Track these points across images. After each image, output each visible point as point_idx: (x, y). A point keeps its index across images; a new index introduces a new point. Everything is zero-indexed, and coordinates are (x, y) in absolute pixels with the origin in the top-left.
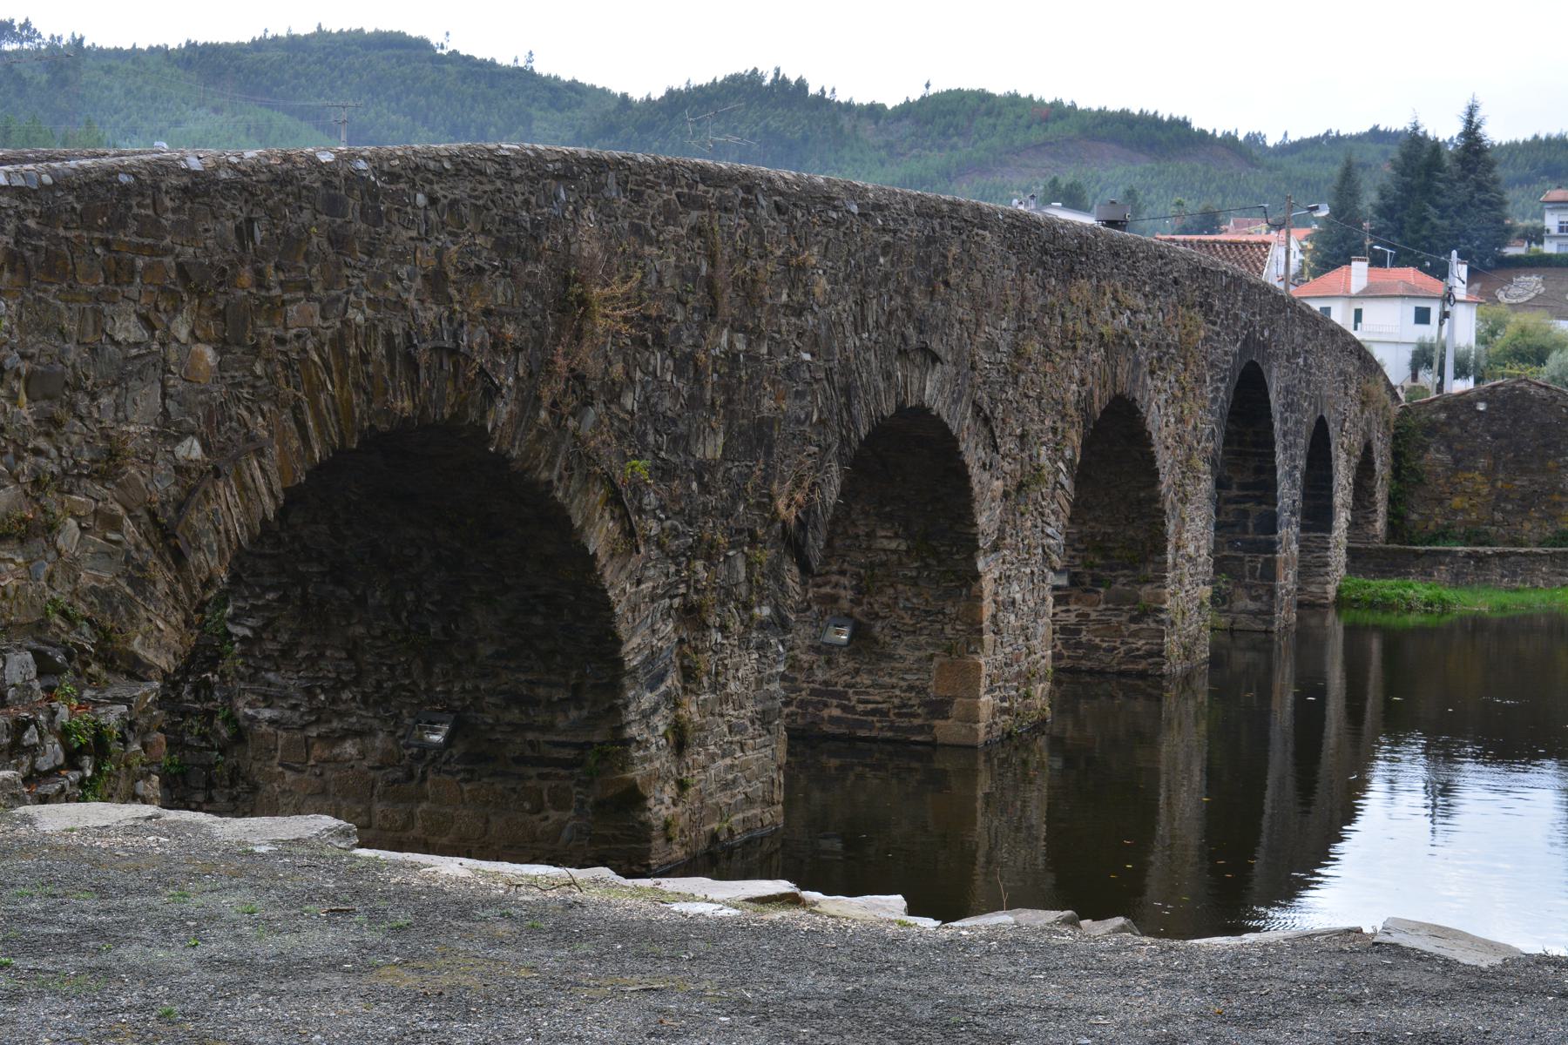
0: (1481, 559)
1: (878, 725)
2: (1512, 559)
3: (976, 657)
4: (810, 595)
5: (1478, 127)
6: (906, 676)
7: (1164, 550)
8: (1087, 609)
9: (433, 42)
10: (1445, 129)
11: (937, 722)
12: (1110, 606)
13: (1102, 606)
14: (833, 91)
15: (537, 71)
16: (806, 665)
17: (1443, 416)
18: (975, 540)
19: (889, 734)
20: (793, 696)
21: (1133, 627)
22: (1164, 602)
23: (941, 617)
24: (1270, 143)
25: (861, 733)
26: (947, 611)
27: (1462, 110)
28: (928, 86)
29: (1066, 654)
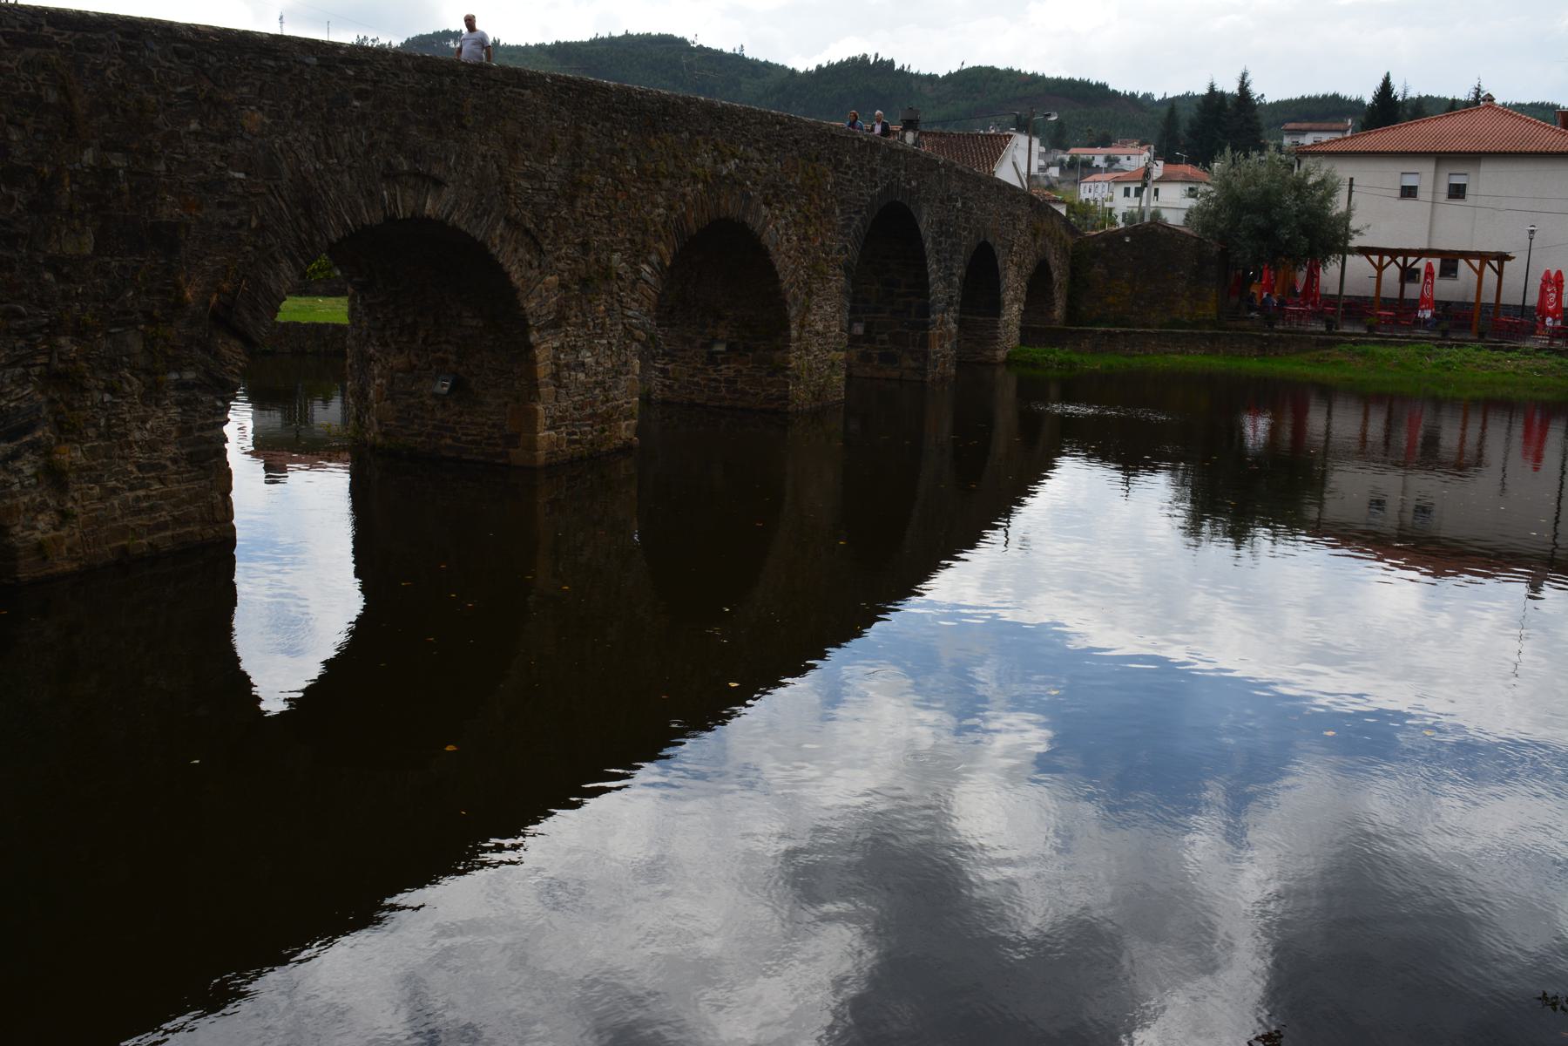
0: (1112, 335)
1: (475, 451)
2: (1133, 335)
3: (534, 404)
4: (430, 358)
5: (1247, 85)
6: (491, 417)
7: (788, 328)
8: (740, 367)
9: (689, 40)
10: (1230, 87)
11: (511, 450)
12: (756, 365)
13: (750, 366)
14: (909, 66)
15: (746, 56)
16: (430, 408)
17: (1103, 245)
18: (526, 320)
19: (482, 458)
20: (423, 429)
21: (769, 379)
22: (790, 363)
23: (511, 375)
24: (1156, 98)
25: (465, 457)
26: (515, 371)
27: (1238, 75)
28: (963, 64)
29: (728, 396)
